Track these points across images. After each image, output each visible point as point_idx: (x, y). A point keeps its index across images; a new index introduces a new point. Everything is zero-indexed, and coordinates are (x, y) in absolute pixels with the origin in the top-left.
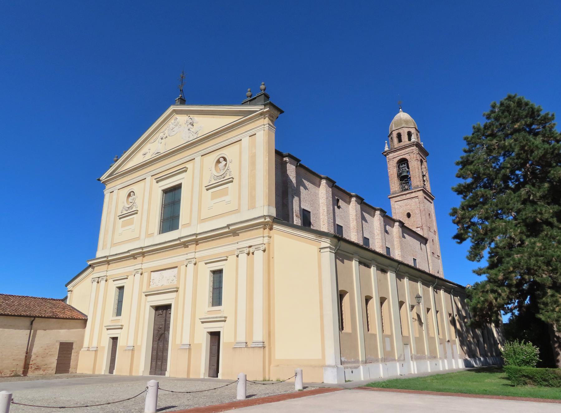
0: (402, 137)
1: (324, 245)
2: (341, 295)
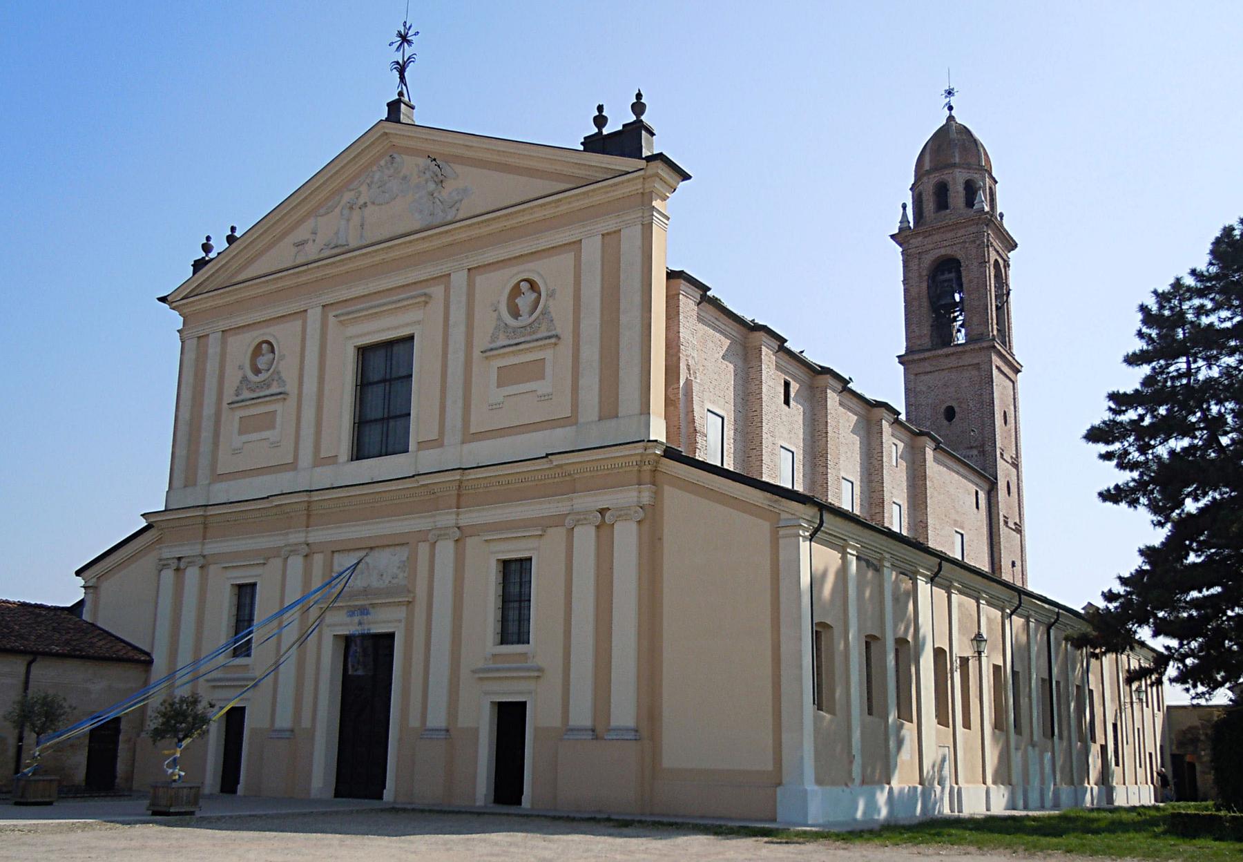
0: (951, 194)
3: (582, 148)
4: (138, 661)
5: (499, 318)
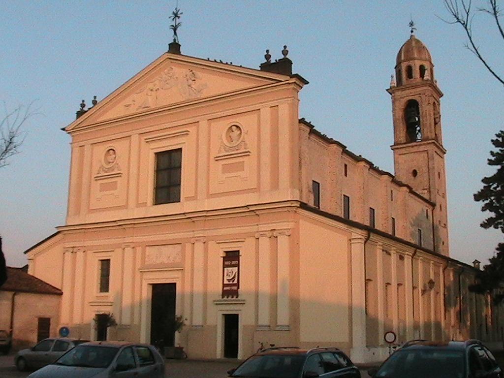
1: (354, 236)
2: (367, 281)
3: (259, 69)
4: (56, 294)
5: (222, 142)
